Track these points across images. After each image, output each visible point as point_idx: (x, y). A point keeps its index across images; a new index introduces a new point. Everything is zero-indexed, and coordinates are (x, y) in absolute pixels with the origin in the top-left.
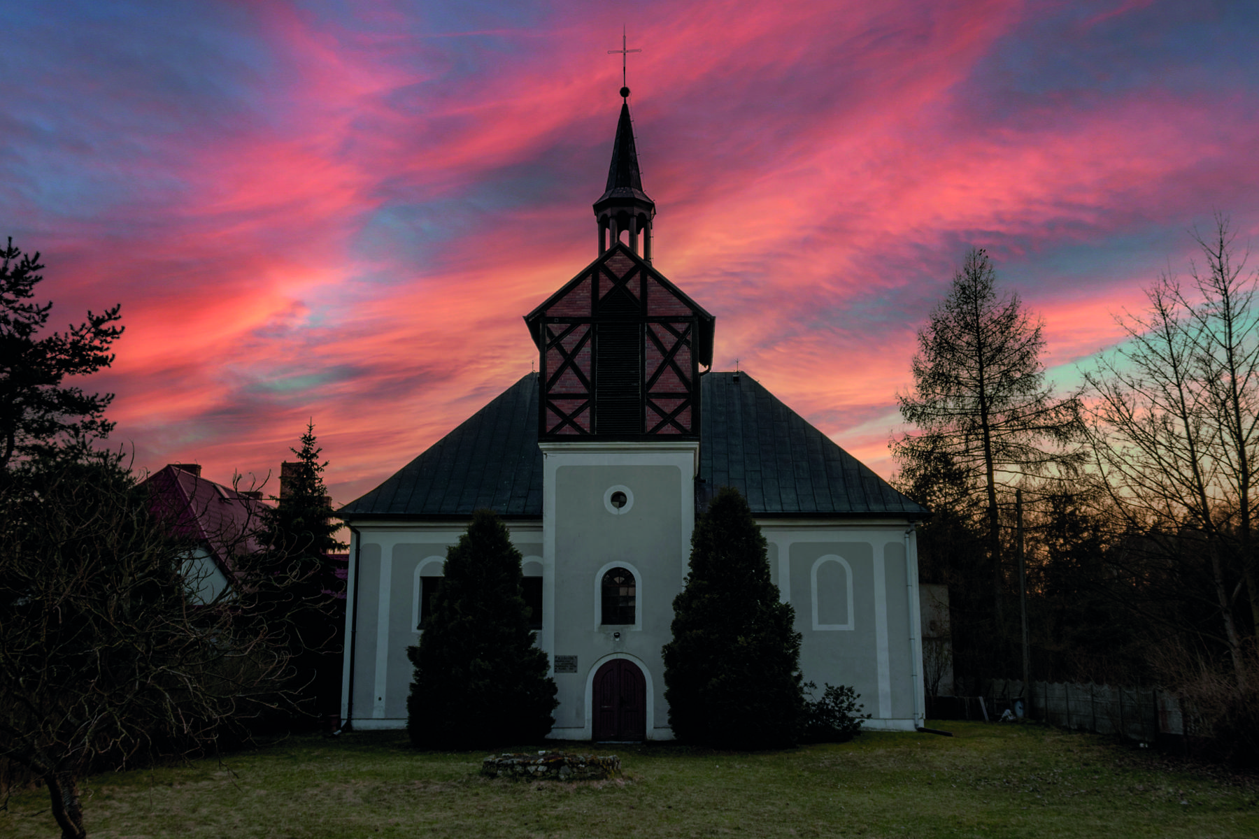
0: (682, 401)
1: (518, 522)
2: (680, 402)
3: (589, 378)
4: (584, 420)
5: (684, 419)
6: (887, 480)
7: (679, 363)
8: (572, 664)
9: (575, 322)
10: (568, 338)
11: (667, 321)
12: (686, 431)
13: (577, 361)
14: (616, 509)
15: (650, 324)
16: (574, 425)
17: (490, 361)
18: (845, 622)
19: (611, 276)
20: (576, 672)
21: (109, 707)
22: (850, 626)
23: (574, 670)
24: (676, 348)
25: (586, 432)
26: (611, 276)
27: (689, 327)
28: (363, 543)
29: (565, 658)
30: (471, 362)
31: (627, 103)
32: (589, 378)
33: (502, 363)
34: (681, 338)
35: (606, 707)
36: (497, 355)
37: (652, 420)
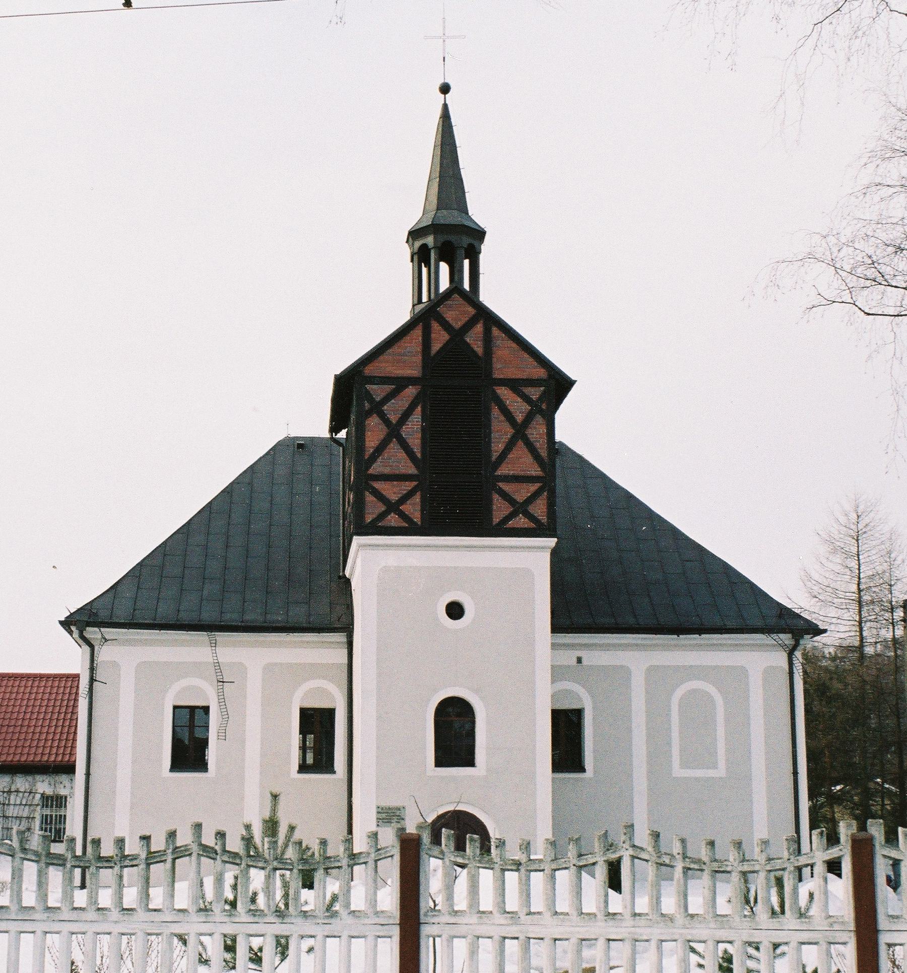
4: (413, 509)
5: (539, 509)
8: (399, 816)
9: (401, 383)
11: (515, 385)
13: (509, 431)
22: (721, 771)
31: (447, 103)
32: (419, 455)
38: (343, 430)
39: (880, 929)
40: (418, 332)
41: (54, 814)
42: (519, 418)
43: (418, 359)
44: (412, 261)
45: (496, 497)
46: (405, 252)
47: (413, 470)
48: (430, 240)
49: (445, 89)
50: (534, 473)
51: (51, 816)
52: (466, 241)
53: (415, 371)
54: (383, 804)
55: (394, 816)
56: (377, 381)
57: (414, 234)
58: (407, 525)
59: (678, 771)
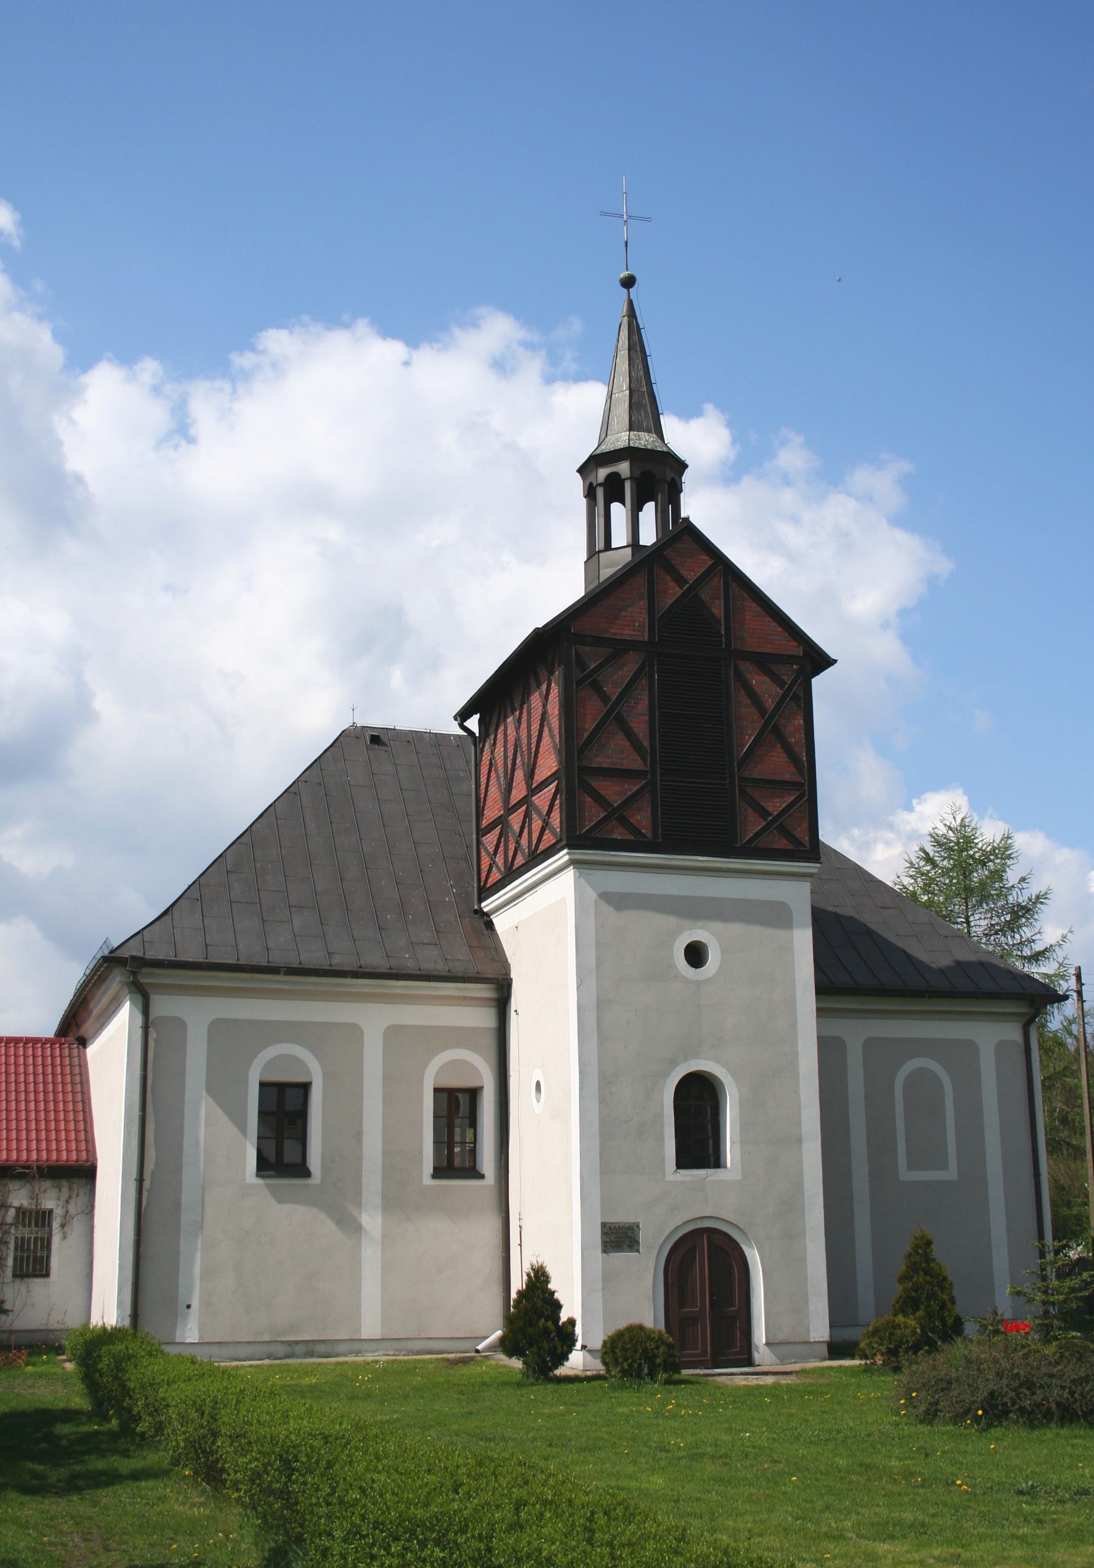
4: (642, 818)
6: (890, 884)
15: (738, 662)
16: (625, 822)
18: (945, 1167)
21: (1007, 1403)
22: (951, 1173)
25: (644, 836)
28: (154, 1013)
31: (631, 297)
37: (753, 825)
38: (475, 716)
39: (75, 1187)
40: (641, 580)
41: (33, 1236)
42: (770, 704)
43: (644, 617)
46: (577, 485)
49: (628, 282)
50: (787, 777)
51: (29, 1239)
52: (670, 474)
57: (595, 461)
58: (633, 838)
59: (906, 1174)
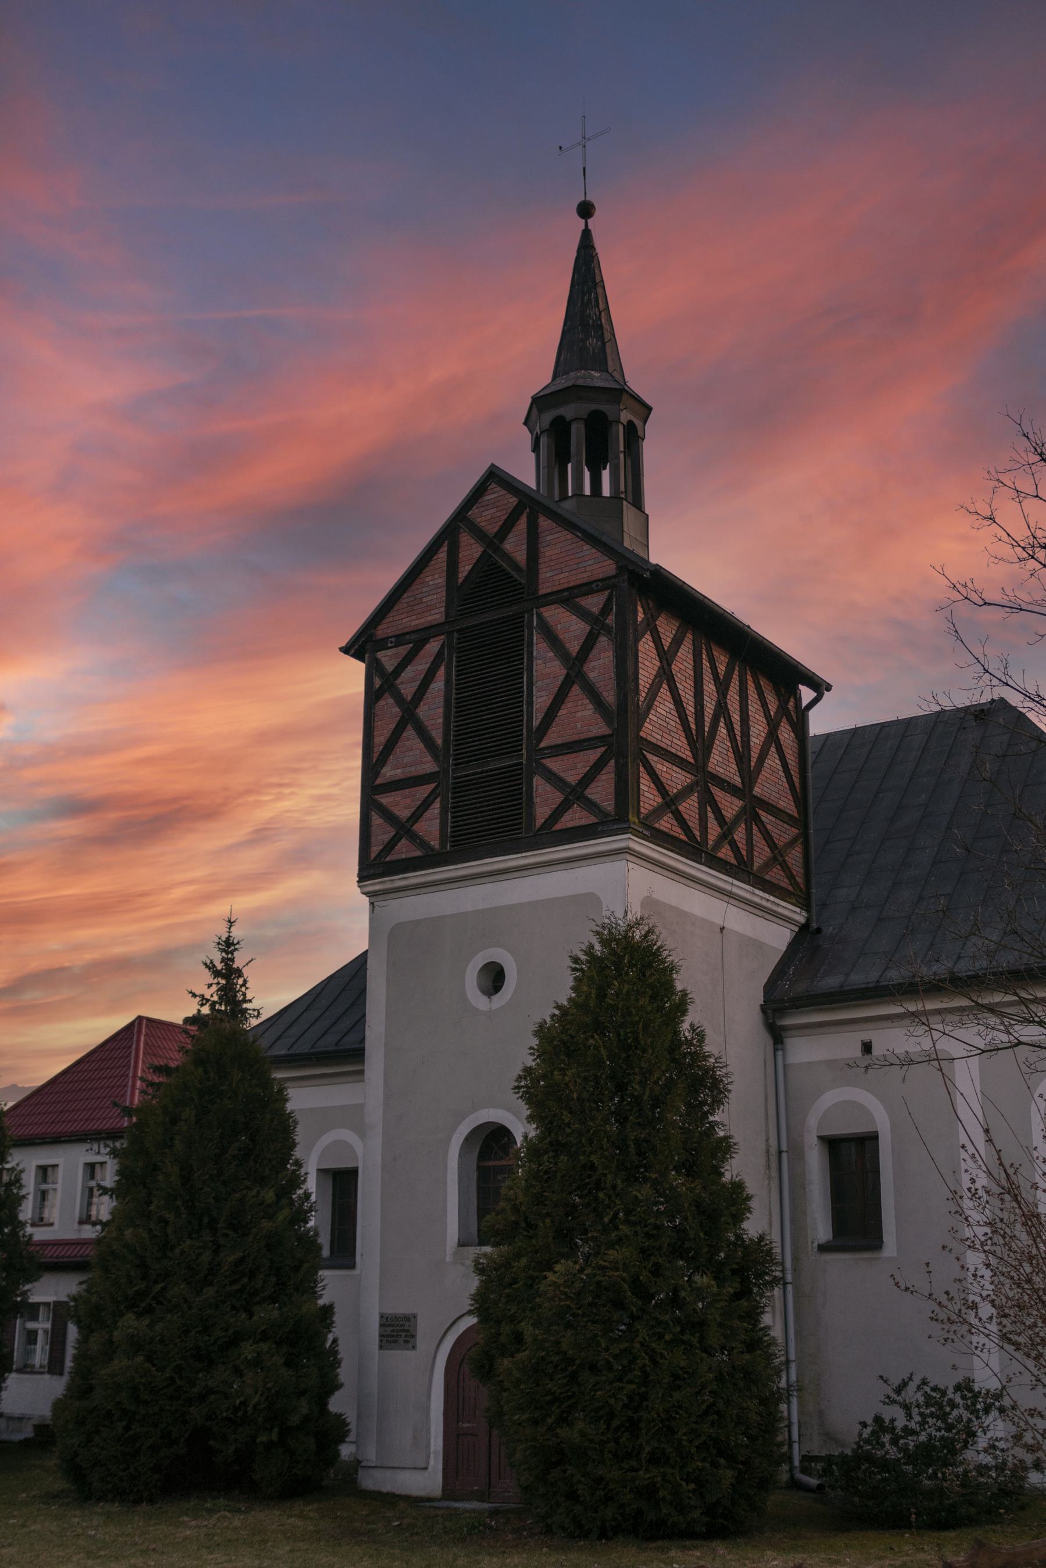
0: (600, 751)
1: (326, 1065)
2: (593, 755)
3: (439, 742)
5: (602, 792)
7: (592, 675)
8: (408, 1331)
9: (419, 638)
10: (409, 672)
11: (568, 597)
12: (608, 815)
13: (422, 712)
14: (485, 999)
15: (542, 610)
17: (276, 791)
19: (479, 534)
20: (414, 1347)
23: (410, 1345)
24: (589, 644)
26: (479, 534)
27: (609, 599)
29: (396, 1318)
30: (249, 792)
31: (590, 228)
32: (439, 742)
33: (292, 793)
34: (597, 625)
35: (466, 1425)
36: (286, 781)
44: (536, 448)
45: (538, 781)
47: (429, 766)
48: (568, 411)
53: (437, 616)
54: (389, 1311)
55: (401, 1331)
56: (391, 642)
